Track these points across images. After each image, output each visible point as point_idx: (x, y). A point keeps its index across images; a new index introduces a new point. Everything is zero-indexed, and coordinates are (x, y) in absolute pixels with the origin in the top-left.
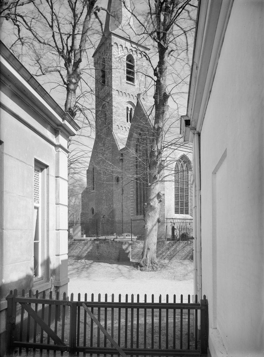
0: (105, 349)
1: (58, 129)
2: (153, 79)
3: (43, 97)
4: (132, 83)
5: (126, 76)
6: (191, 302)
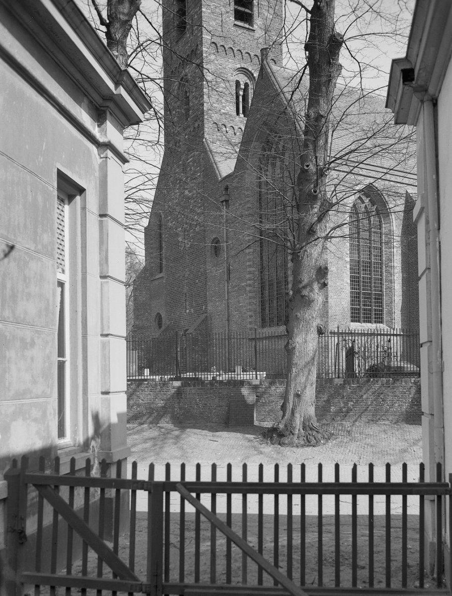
0: (227, 588)
1: (104, 107)
2: (303, 6)
3: (77, 30)
4: (247, 26)
5: (232, 9)
6: (427, 480)
